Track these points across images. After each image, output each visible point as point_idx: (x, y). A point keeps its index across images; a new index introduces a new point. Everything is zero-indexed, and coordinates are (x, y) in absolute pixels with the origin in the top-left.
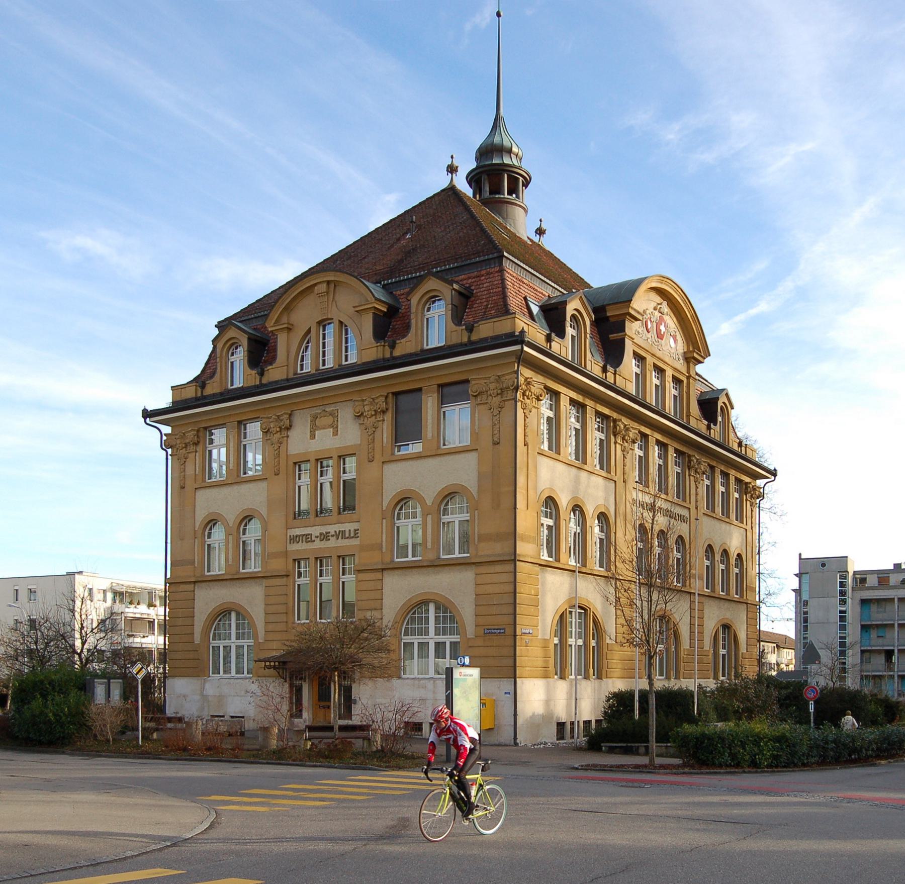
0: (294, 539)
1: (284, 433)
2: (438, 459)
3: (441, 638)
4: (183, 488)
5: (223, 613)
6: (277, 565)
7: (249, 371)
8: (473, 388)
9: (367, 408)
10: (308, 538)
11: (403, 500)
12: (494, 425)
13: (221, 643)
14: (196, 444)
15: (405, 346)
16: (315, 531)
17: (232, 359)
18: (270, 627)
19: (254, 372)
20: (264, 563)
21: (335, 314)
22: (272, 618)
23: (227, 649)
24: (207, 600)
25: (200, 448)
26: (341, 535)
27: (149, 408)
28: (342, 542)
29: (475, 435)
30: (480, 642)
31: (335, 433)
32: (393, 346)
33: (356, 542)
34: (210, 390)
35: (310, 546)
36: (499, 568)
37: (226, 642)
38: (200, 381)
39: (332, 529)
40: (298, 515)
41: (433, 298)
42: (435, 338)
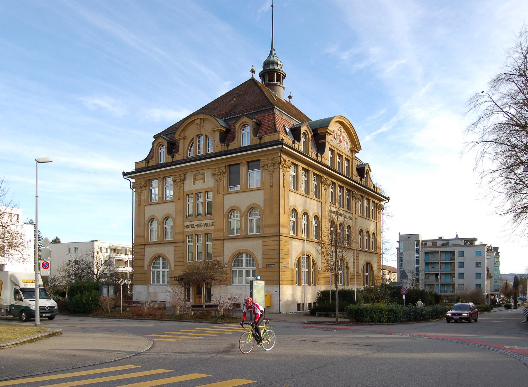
0: (187, 227)
1: (182, 182)
3: (248, 268)
5: (156, 258)
6: (180, 238)
7: (168, 156)
9: (217, 172)
10: (192, 226)
11: (232, 210)
13: (156, 271)
14: (145, 187)
15: (233, 146)
16: (195, 223)
17: (160, 151)
18: (177, 264)
19: (169, 156)
21: (204, 132)
22: (177, 260)
24: (150, 252)
25: (147, 188)
26: (206, 225)
29: (262, 183)
30: (264, 270)
33: (212, 228)
36: (272, 239)
37: (240, 269)
38: (147, 160)
39: (202, 222)
40: (188, 216)
42: (246, 143)
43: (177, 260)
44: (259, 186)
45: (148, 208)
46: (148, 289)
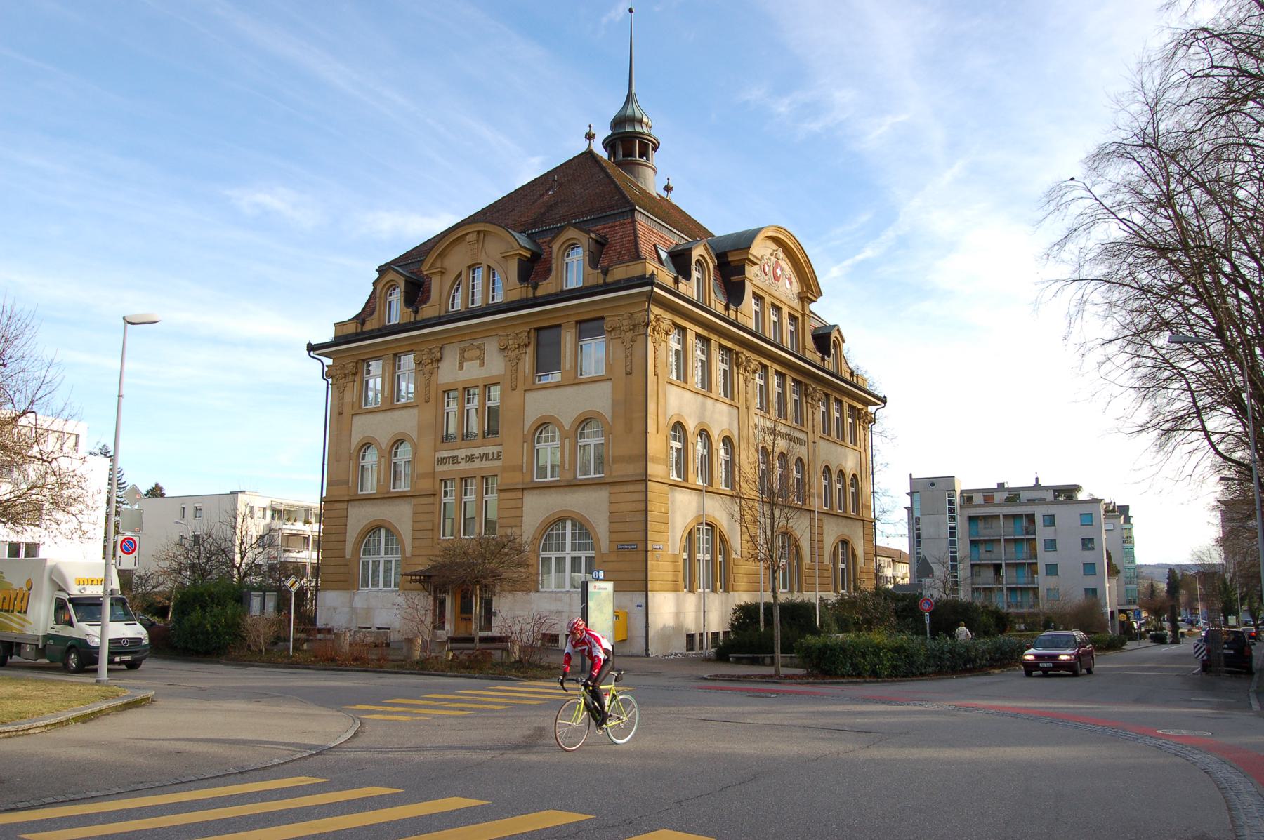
0: (442, 461)
1: (435, 365)
2: (576, 388)
3: (577, 554)
4: (341, 414)
6: (426, 485)
7: (405, 309)
8: (607, 324)
10: (454, 460)
11: (543, 425)
12: (627, 357)
13: (371, 558)
14: (355, 374)
15: (546, 287)
16: (461, 453)
17: (390, 299)
20: (413, 483)
22: (419, 535)
23: (376, 563)
24: (359, 517)
25: (358, 378)
26: (484, 457)
27: (314, 343)
28: (485, 464)
30: (613, 558)
31: (482, 365)
32: (535, 287)
34: (369, 326)
35: (456, 467)
36: (631, 488)
37: (376, 557)
38: (360, 319)
40: (446, 438)
41: (572, 246)
42: (574, 280)
43: (419, 535)
44: (602, 372)
45: (358, 421)
46: (352, 601)
